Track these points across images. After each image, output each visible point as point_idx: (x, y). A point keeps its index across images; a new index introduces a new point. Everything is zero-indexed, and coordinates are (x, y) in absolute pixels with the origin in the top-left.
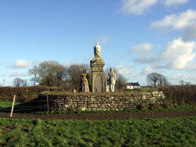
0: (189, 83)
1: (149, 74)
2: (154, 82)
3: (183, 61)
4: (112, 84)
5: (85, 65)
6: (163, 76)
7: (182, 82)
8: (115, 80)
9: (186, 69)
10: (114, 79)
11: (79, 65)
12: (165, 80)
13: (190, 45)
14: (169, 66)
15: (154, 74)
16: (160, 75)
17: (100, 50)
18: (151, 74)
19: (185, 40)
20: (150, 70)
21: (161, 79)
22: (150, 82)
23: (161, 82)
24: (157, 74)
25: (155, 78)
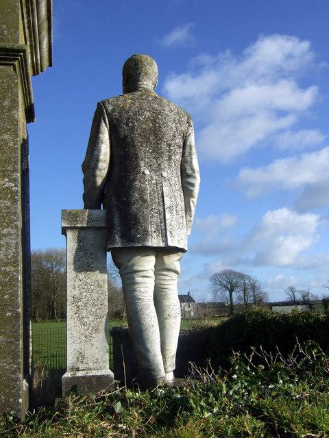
0: (308, 293)
1: (216, 274)
2: (227, 293)
3: (291, 248)
4: (155, 241)
5: (57, 253)
6: (249, 278)
7: (292, 290)
8: (106, 124)
9: (296, 267)
10: (171, 175)
11: (168, 299)
12: (254, 287)
13: (311, 220)
14: (260, 260)
15: (228, 274)
16: (242, 276)
17: (103, 124)
18: (220, 275)
19: (300, 210)
20: (219, 266)
21: (245, 284)
22: (219, 293)
23: (245, 291)
24: (235, 274)
25: (231, 283)
